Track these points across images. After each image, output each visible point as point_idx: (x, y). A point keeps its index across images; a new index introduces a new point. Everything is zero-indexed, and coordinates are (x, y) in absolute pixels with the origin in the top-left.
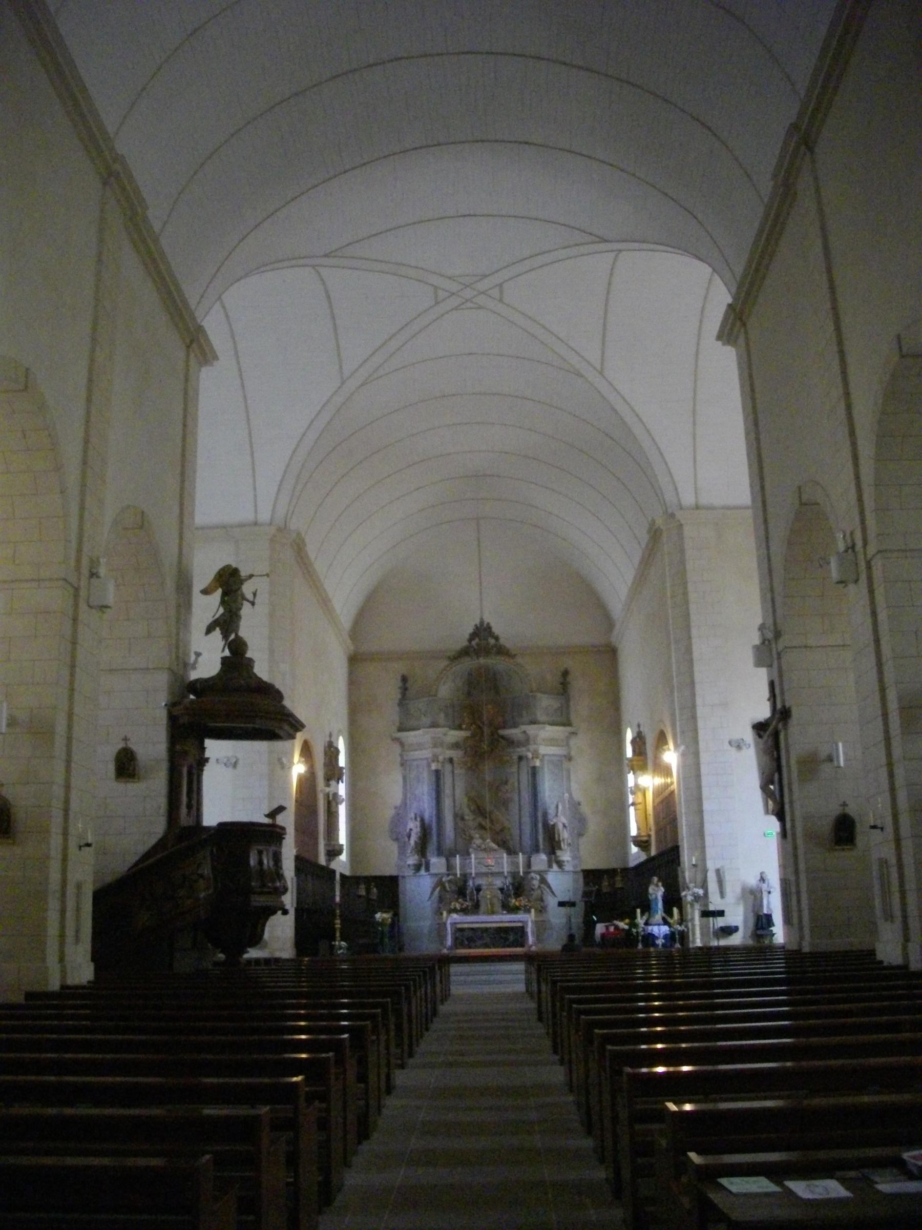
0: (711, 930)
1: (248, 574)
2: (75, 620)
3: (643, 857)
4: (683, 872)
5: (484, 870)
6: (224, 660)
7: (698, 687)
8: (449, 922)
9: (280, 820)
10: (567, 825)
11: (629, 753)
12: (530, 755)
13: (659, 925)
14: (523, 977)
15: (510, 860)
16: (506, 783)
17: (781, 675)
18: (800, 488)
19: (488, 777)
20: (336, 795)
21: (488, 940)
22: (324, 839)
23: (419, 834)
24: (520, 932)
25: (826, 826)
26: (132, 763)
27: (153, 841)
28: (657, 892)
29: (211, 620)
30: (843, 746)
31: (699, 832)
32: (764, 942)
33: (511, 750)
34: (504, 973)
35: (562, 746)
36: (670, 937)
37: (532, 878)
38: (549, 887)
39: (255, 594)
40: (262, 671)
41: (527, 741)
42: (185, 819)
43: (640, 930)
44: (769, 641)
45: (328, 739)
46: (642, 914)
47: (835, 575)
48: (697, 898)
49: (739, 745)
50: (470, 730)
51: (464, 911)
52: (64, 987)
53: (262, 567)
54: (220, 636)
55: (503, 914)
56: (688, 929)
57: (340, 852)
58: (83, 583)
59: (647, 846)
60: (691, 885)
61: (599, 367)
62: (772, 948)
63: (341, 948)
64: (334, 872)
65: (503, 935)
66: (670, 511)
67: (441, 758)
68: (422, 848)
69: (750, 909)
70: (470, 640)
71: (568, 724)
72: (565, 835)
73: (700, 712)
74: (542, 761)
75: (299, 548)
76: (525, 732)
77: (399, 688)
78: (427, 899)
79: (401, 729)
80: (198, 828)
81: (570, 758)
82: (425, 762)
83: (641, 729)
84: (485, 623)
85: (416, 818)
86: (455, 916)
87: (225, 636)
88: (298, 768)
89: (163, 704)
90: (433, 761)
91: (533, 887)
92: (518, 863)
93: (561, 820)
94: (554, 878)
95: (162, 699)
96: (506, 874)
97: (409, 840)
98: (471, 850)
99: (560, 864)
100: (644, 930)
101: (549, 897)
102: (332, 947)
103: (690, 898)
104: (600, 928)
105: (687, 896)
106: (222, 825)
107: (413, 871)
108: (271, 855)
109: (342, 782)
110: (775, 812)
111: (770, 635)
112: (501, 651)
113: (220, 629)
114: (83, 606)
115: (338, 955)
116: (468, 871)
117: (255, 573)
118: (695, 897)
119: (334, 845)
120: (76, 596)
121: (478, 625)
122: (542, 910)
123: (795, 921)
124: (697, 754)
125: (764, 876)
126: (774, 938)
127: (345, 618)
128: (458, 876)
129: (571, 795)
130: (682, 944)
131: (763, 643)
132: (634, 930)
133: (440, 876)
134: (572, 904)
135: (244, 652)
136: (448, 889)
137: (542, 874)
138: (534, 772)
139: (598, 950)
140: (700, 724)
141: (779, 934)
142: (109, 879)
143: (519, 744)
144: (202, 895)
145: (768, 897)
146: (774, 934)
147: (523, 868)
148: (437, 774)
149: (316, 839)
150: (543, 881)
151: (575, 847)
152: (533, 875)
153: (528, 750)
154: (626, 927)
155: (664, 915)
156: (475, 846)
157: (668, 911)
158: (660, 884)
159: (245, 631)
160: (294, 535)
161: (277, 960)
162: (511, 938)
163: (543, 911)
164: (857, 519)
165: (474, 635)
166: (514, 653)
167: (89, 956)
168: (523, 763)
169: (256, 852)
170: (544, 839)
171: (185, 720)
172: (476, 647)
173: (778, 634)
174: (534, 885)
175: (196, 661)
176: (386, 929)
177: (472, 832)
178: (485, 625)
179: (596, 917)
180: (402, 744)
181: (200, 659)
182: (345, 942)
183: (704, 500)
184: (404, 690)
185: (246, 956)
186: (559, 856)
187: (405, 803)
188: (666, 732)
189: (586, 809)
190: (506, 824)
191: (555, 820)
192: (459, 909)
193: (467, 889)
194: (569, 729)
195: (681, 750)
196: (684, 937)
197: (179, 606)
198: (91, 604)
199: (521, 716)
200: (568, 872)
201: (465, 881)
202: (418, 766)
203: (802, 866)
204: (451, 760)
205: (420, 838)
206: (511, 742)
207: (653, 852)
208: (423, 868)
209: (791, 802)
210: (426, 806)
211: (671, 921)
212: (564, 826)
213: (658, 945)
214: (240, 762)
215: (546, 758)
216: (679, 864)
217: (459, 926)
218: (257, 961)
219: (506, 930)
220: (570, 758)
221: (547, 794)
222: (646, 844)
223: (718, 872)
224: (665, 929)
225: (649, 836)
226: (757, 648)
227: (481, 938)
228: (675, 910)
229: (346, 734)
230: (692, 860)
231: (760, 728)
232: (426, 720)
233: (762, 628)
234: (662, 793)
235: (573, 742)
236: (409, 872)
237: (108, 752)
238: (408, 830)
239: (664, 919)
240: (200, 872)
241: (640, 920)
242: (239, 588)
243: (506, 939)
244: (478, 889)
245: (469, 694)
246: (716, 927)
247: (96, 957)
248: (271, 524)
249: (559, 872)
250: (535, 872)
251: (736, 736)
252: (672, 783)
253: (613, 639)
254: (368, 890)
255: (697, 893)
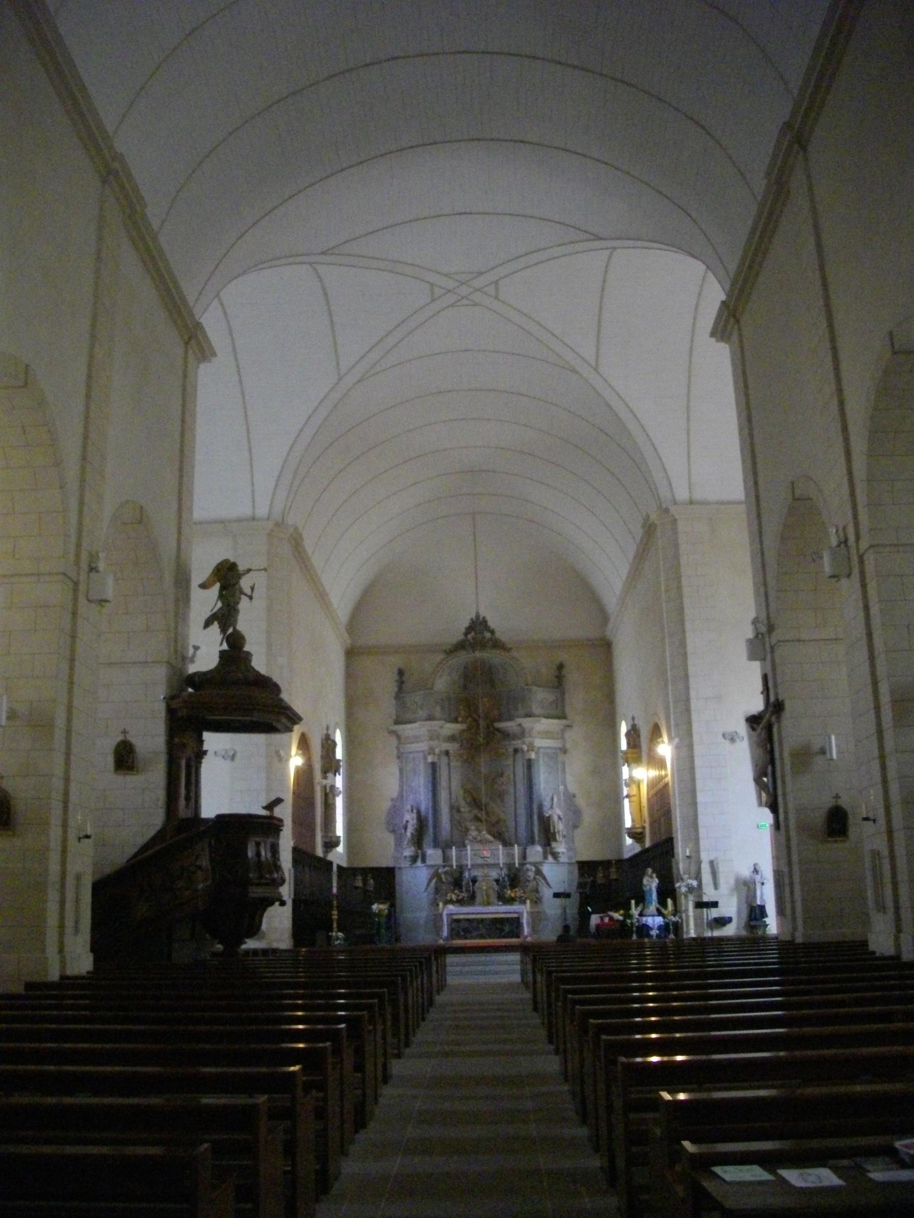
0: (705, 921)
1: (246, 568)
2: (74, 614)
3: (638, 849)
4: (677, 864)
5: (480, 861)
6: (222, 654)
7: (692, 681)
8: (445, 913)
9: (278, 812)
10: (562, 817)
11: (624, 745)
12: (525, 748)
13: (653, 916)
14: (519, 967)
15: (505, 851)
16: (502, 775)
17: (774, 669)
18: (793, 483)
19: (484, 770)
20: (333, 787)
21: (483, 931)
22: (322, 830)
23: (416, 826)
24: (516, 923)
25: (819, 818)
26: (131, 755)
27: (151, 833)
28: (651, 883)
29: (209, 614)
30: (836, 739)
31: (693, 824)
32: (757, 933)
33: (507, 743)
34: (499, 963)
35: (558, 739)
36: (665, 928)
37: (528, 870)
38: (544, 878)
39: (252, 589)
40: (259, 664)
41: (522, 734)
42: (183, 811)
43: (635, 920)
44: (762, 635)
45: (325, 732)
46: (637, 905)
47: (827, 569)
48: (691, 889)
49: (732, 738)
50: (466, 723)
51: (460, 902)
52: (63, 977)
53: (260, 562)
54: (219, 630)
55: (498, 905)
56: (682, 920)
57: (337, 844)
58: (83, 577)
59: (642, 838)
60: (685, 877)
61: (593, 364)
62: (765, 939)
63: (338, 939)
64: (331, 863)
65: (498, 926)
66: (664, 506)
67: (437, 751)
68: (418, 840)
69: (744, 900)
70: (466, 634)
71: (563, 717)
72: (560, 827)
73: (694, 705)
74: (537, 753)
75: (297, 543)
76: (520, 725)
77: (395, 681)
78: (423, 890)
79: (397, 722)
80: (196, 820)
81: (565, 751)
82: (421, 754)
83: (636, 722)
84: (481, 617)
85: (412, 810)
86: (451, 907)
87: (223, 629)
88: (296, 761)
89: (162, 697)
90: (430, 754)
91: (529, 879)
92: (513, 855)
93: (556, 812)
94: (549, 869)
95: (161, 692)
96: (501, 865)
97: (406, 832)
98: (467, 842)
99: (555, 856)
100: (638, 921)
101: (545, 888)
102: (329, 938)
103: (684, 889)
104: (595, 919)
105: (681, 887)
106: (220, 817)
107: (410, 863)
108: (268, 846)
109: (339, 774)
110: (769, 804)
111: (763, 629)
112: (497, 644)
113: (219, 623)
115: (335, 946)
116: (464, 862)
117: (253, 568)
118: (689, 888)
119: (331, 837)
120: (76, 590)
121: (474, 619)
122: (537, 901)
123: (788, 912)
124: (691, 747)
125: (757, 867)
126: (767, 929)
127: (342, 612)
128: (454, 867)
129: (566, 787)
130: (676, 935)
131: (757, 637)
132: (629, 921)
133: (436, 867)
134: (567, 895)
135: (242, 646)
136: (444, 880)
137: (537, 865)
138: (529, 764)
139: (592, 941)
140: (694, 716)
141: (772, 925)
142: (108, 870)
143: (515, 737)
144: (200, 886)
145: (762, 888)
146: (767, 925)
147: (519, 859)
148: (434, 766)
149: (313, 831)
150: (539, 872)
151: (570, 839)
152: (528, 866)
153: (524, 743)
154: (621, 918)
155: (658, 906)
156: (471, 837)
157: (662, 902)
158: (654, 875)
159: (243, 625)
160: (292, 530)
161: (275, 951)
162: (507, 928)
163: (538, 902)
164: (850, 514)
165: (470, 629)
166: (509, 646)
167: (88, 947)
168: (519, 756)
169: (254, 843)
171: (183, 713)
172: (472, 641)
173: (771, 628)
174: (529, 877)
175: (194, 655)
176: (383, 920)
177: (468, 824)
178: (481, 619)
179: (591, 908)
180: (398, 737)
181: (198, 653)
182: (342, 933)
183: (698, 496)
184: (401, 683)
185: (244, 947)
186: (554, 848)
187: (401, 795)
188: (660, 725)
189: (581, 801)
190: (502, 816)
191: (550, 812)
192: (455, 900)
193: (463, 880)
194: (564, 722)
195: (675, 743)
196: (678, 928)
197: (177, 600)
198: (90, 598)
199: (517, 709)
200: (563, 863)
201: (461, 873)
202: (414, 759)
203: (795, 858)
204: (447, 753)
205: (416, 830)
206: (506, 735)
207: (648, 844)
208: (419, 860)
209: (784, 794)
210: (422, 798)
211: (665, 912)
212: (560, 818)
213: (652, 936)
214: (238, 755)
215: (541, 750)
216: (673, 856)
217: (455, 917)
218: (255, 952)
219: (502, 921)
220: (565, 751)
221: (542, 786)
222: (641, 836)
223: (712, 863)
224: (659, 920)
225: (644, 828)
226: (750, 642)
227: (477, 929)
228: (669, 902)
229: (343, 726)
230: (686, 852)
231: (753, 721)
232: (422, 713)
233: (755, 622)
234: (656, 785)
235: (568, 734)
236: (406, 864)
237: (107, 745)
238: (404, 822)
239: (658, 910)
240: (198, 863)
241: (635, 911)
242: (237, 583)
243: (502, 930)
244: (474, 880)
245: (465, 687)
246: (710, 918)
247: (96, 948)
248: (268, 519)
249: (554, 863)
250: (530, 863)
251: (730, 729)
252: (666, 776)
253: (608, 633)
254: (365, 882)
255: (691, 885)
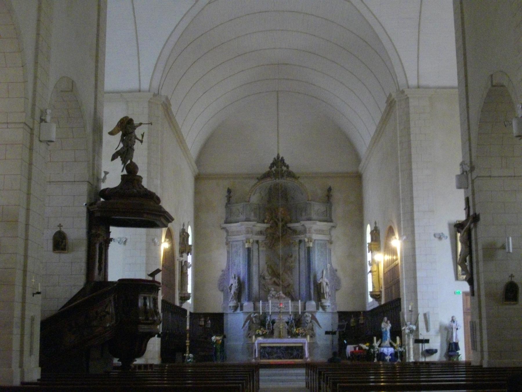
0: (421, 351)
1: (138, 123)
2: (31, 149)
3: (376, 305)
4: (403, 315)
5: (277, 310)
6: (123, 177)
7: (415, 200)
8: (256, 342)
10: (328, 284)
11: (368, 239)
12: (306, 240)
13: (388, 347)
14: (304, 378)
15: (293, 305)
16: (291, 256)
17: (473, 194)
18: (492, 76)
19: (281, 253)
20: (186, 262)
22: (179, 289)
23: (237, 288)
24: (300, 349)
25: (500, 289)
26: (64, 241)
27: (76, 291)
28: (387, 326)
29: (114, 151)
30: (512, 239)
31: (414, 291)
32: (453, 360)
33: (295, 236)
34: (292, 375)
35: (327, 235)
36: (395, 355)
37: (307, 316)
38: (317, 322)
39: (143, 136)
41: (304, 231)
42: (97, 276)
43: (376, 350)
44: (466, 172)
45: (182, 227)
46: (377, 340)
47: (515, 130)
48: (411, 331)
49: (440, 237)
50: (270, 223)
51: (264, 336)
52: (23, 383)
53: (144, 119)
54: (121, 162)
55: (288, 338)
56: (406, 351)
58: (36, 126)
59: (379, 298)
60: (408, 323)
62: (458, 363)
63: (189, 358)
64: (185, 311)
65: (290, 351)
66: (401, 89)
67: (251, 240)
68: (238, 296)
69: (445, 339)
70: (271, 168)
71: (331, 221)
72: (327, 289)
73: (416, 215)
74: (314, 243)
75: (167, 107)
76: (303, 225)
77: (226, 196)
78: (241, 328)
79: (226, 222)
80: (106, 283)
81: (331, 242)
82: (241, 243)
83: (377, 225)
84: (281, 157)
85: (235, 277)
86: (260, 339)
87: (124, 162)
88: (165, 245)
89: (84, 204)
90: (247, 242)
91: (307, 322)
92: (298, 307)
93: (325, 281)
94: (320, 316)
95: (84, 201)
96: (290, 313)
97: (231, 291)
98: (269, 298)
99: (324, 308)
100: (378, 350)
101: (317, 327)
102: (184, 358)
103: (407, 331)
104: (350, 348)
105: (406, 330)
106: (121, 281)
107: (233, 310)
108: (152, 299)
109: (191, 254)
110: (467, 279)
111: (468, 169)
112: (291, 175)
113: (121, 157)
114: (36, 142)
115: (188, 363)
116: (267, 311)
117: (143, 123)
118: (411, 331)
119: (185, 294)
120: (32, 134)
121: (276, 158)
122: (312, 336)
123: (479, 348)
124: (413, 242)
125: (454, 318)
126: (459, 357)
128: (261, 314)
130: (401, 360)
131: (463, 173)
132: (372, 350)
133: (249, 314)
134: (333, 333)
135: (136, 173)
136: (255, 322)
137: (313, 313)
138: (309, 250)
139: (349, 363)
140: (416, 223)
141: (463, 355)
143: (301, 233)
144: (108, 325)
145: (456, 332)
146: (459, 355)
147: (301, 310)
148: (249, 250)
149: (174, 290)
150: (314, 318)
151: (333, 298)
152: (307, 314)
153: (306, 237)
154: (367, 348)
155: (391, 341)
156: (271, 295)
157: (393, 339)
158: (389, 322)
160: (164, 99)
161: (151, 366)
162: (295, 353)
163: (313, 336)
165: (273, 164)
166: (297, 175)
167: (37, 364)
168: (302, 244)
169: (142, 298)
170: (314, 294)
171: (98, 214)
172: (274, 172)
173: (472, 169)
174: (308, 321)
175: (105, 178)
176: (218, 347)
177: (270, 286)
179: (346, 341)
180: (227, 231)
181: (107, 176)
182: (192, 354)
183: (423, 83)
184: (229, 198)
185: (135, 363)
186: (323, 303)
187: (228, 268)
188: (393, 228)
189: (340, 274)
190: (291, 282)
191: (321, 280)
192: (261, 334)
193: (266, 322)
194: (331, 224)
195: (403, 239)
196: (402, 355)
197: (94, 142)
198: (41, 139)
199: (301, 215)
200: (328, 312)
201: (265, 317)
203: (484, 315)
204: (257, 242)
205: (237, 290)
207: (383, 302)
208: (239, 308)
209: (478, 273)
211: (395, 345)
212: (327, 284)
213: (386, 360)
214: (128, 241)
215: (316, 242)
216: (400, 310)
217: (262, 345)
218: (140, 366)
219: (292, 348)
220: (331, 242)
221: (316, 263)
222: (379, 297)
223: (425, 315)
224: (391, 350)
225: (381, 292)
226: (459, 177)
227: (277, 353)
228: (398, 338)
229: (192, 223)
230: (409, 308)
231: (459, 226)
232: (242, 217)
233: (462, 164)
234: (390, 265)
235: (334, 232)
236: (230, 311)
237: (50, 234)
238: (230, 285)
239: (391, 344)
241: (376, 344)
242: (133, 132)
243: (292, 354)
244: (273, 322)
245: (269, 201)
246: (424, 349)
247: (42, 364)
248: (149, 91)
249: (323, 312)
250: (309, 312)
251: (439, 231)
252: (397, 259)
253: (360, 169)
254: (205, 322)
255: (412, 328)
